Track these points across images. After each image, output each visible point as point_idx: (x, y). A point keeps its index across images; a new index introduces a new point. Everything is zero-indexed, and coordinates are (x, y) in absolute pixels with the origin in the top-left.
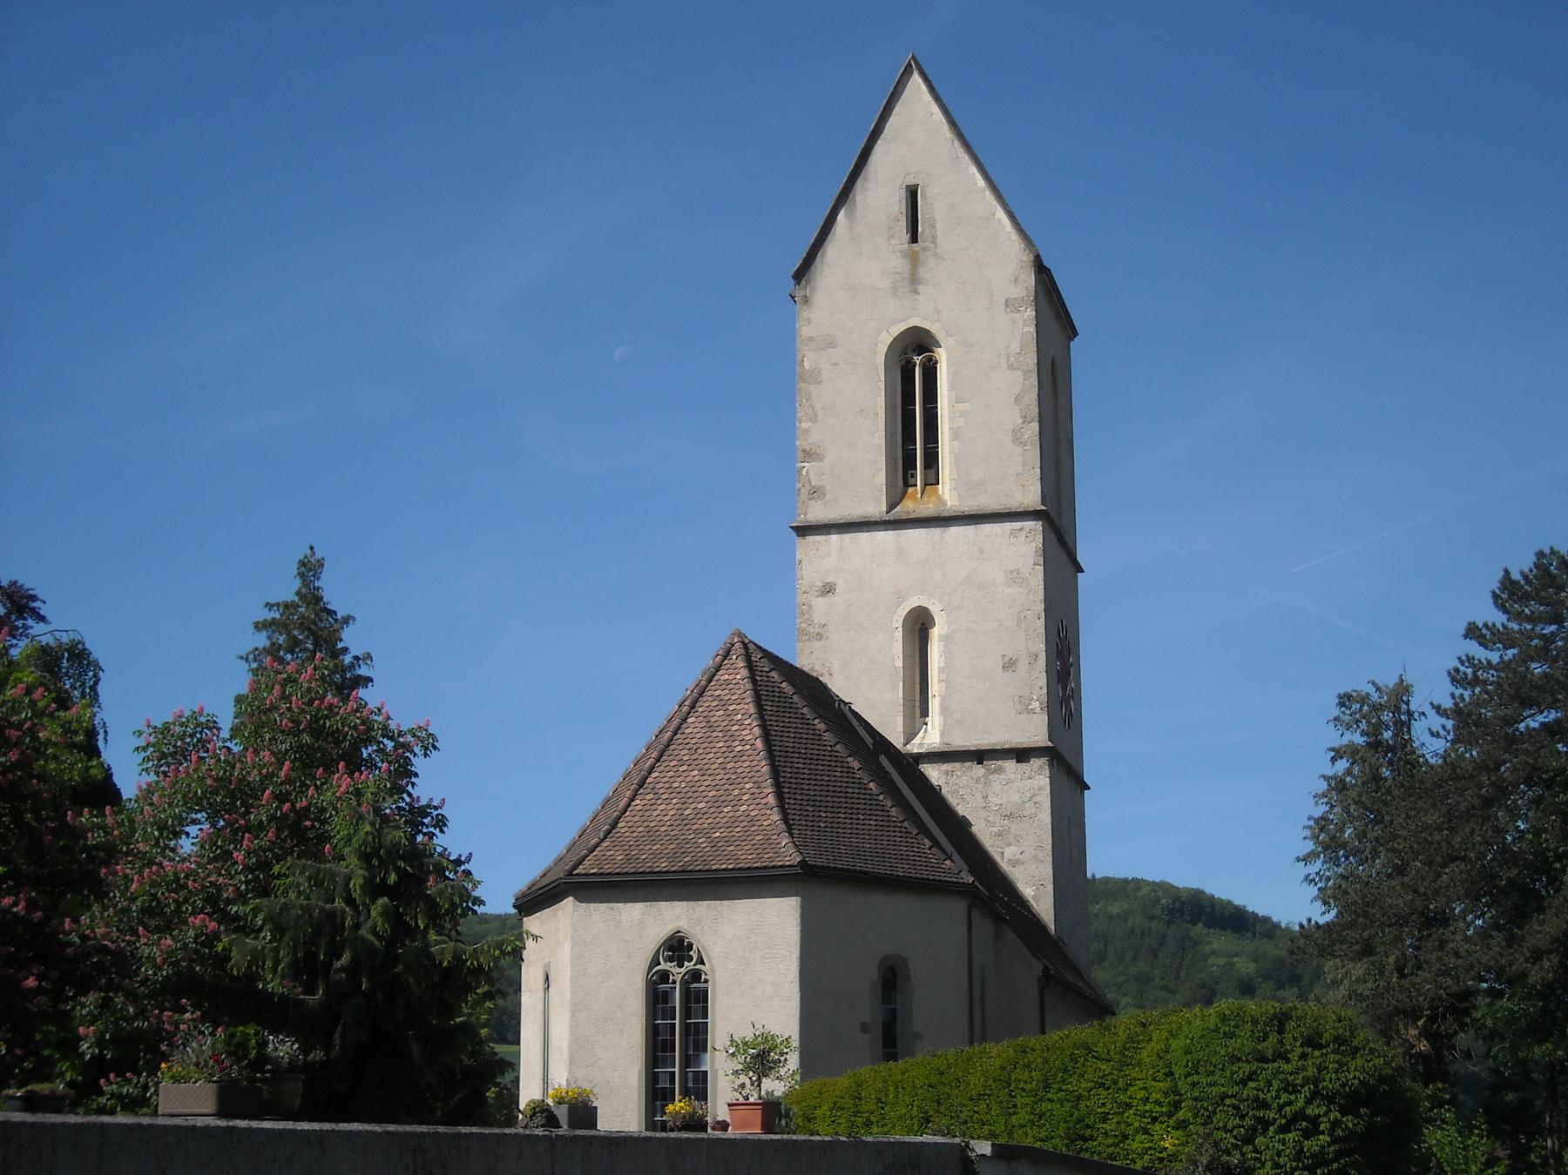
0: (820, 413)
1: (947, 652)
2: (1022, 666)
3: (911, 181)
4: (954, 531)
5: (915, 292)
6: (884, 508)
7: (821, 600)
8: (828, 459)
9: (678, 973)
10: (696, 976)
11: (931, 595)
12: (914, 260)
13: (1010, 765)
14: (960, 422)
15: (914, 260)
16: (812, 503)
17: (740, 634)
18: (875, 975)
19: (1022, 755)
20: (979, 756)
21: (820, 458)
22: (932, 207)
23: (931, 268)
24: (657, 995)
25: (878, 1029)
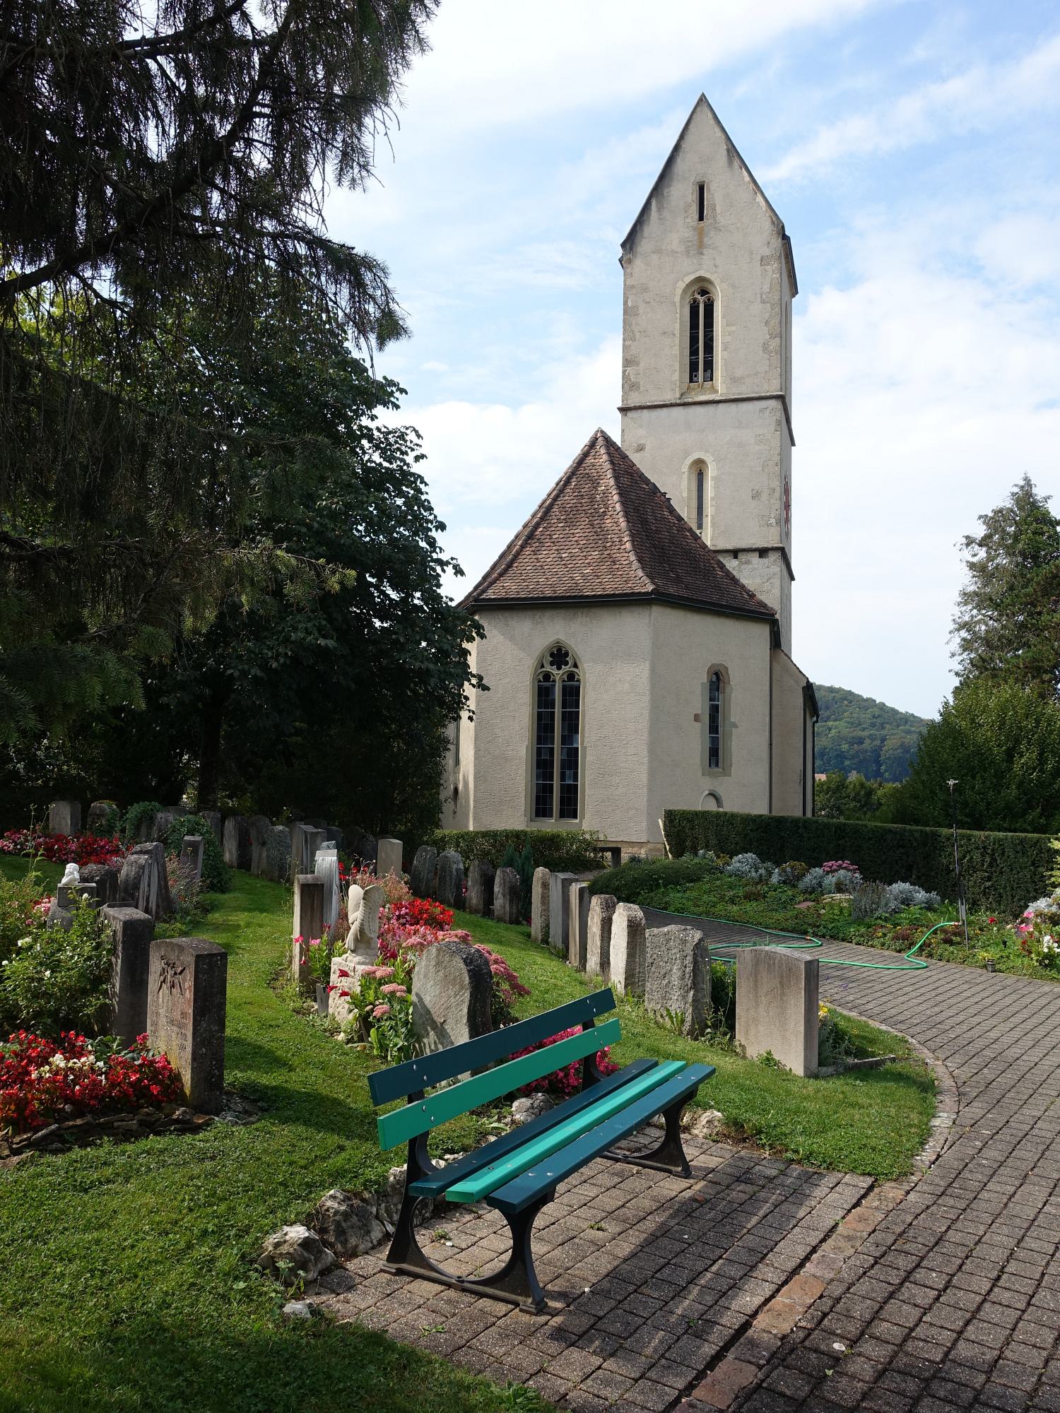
0: (638, 335)
1: (716, 487)
2: (764, 496)
3: (699, 179)
4: (721, 405)
6: (678, 395)
7: (638, 455)
8: (642, 365)
9: (558, 674)
10: (571, 676)
11: (707, 451)
12: (701, 234)
13: (754, 558)
14: (729, 339)
15: (701, 234)
17: (602, 432)
18: (704, 678)
19: (763, 552)
21: (638, 364)
22: (715, 196)
23: (713, 238)
24: (543, 693)
25: (706, 719)
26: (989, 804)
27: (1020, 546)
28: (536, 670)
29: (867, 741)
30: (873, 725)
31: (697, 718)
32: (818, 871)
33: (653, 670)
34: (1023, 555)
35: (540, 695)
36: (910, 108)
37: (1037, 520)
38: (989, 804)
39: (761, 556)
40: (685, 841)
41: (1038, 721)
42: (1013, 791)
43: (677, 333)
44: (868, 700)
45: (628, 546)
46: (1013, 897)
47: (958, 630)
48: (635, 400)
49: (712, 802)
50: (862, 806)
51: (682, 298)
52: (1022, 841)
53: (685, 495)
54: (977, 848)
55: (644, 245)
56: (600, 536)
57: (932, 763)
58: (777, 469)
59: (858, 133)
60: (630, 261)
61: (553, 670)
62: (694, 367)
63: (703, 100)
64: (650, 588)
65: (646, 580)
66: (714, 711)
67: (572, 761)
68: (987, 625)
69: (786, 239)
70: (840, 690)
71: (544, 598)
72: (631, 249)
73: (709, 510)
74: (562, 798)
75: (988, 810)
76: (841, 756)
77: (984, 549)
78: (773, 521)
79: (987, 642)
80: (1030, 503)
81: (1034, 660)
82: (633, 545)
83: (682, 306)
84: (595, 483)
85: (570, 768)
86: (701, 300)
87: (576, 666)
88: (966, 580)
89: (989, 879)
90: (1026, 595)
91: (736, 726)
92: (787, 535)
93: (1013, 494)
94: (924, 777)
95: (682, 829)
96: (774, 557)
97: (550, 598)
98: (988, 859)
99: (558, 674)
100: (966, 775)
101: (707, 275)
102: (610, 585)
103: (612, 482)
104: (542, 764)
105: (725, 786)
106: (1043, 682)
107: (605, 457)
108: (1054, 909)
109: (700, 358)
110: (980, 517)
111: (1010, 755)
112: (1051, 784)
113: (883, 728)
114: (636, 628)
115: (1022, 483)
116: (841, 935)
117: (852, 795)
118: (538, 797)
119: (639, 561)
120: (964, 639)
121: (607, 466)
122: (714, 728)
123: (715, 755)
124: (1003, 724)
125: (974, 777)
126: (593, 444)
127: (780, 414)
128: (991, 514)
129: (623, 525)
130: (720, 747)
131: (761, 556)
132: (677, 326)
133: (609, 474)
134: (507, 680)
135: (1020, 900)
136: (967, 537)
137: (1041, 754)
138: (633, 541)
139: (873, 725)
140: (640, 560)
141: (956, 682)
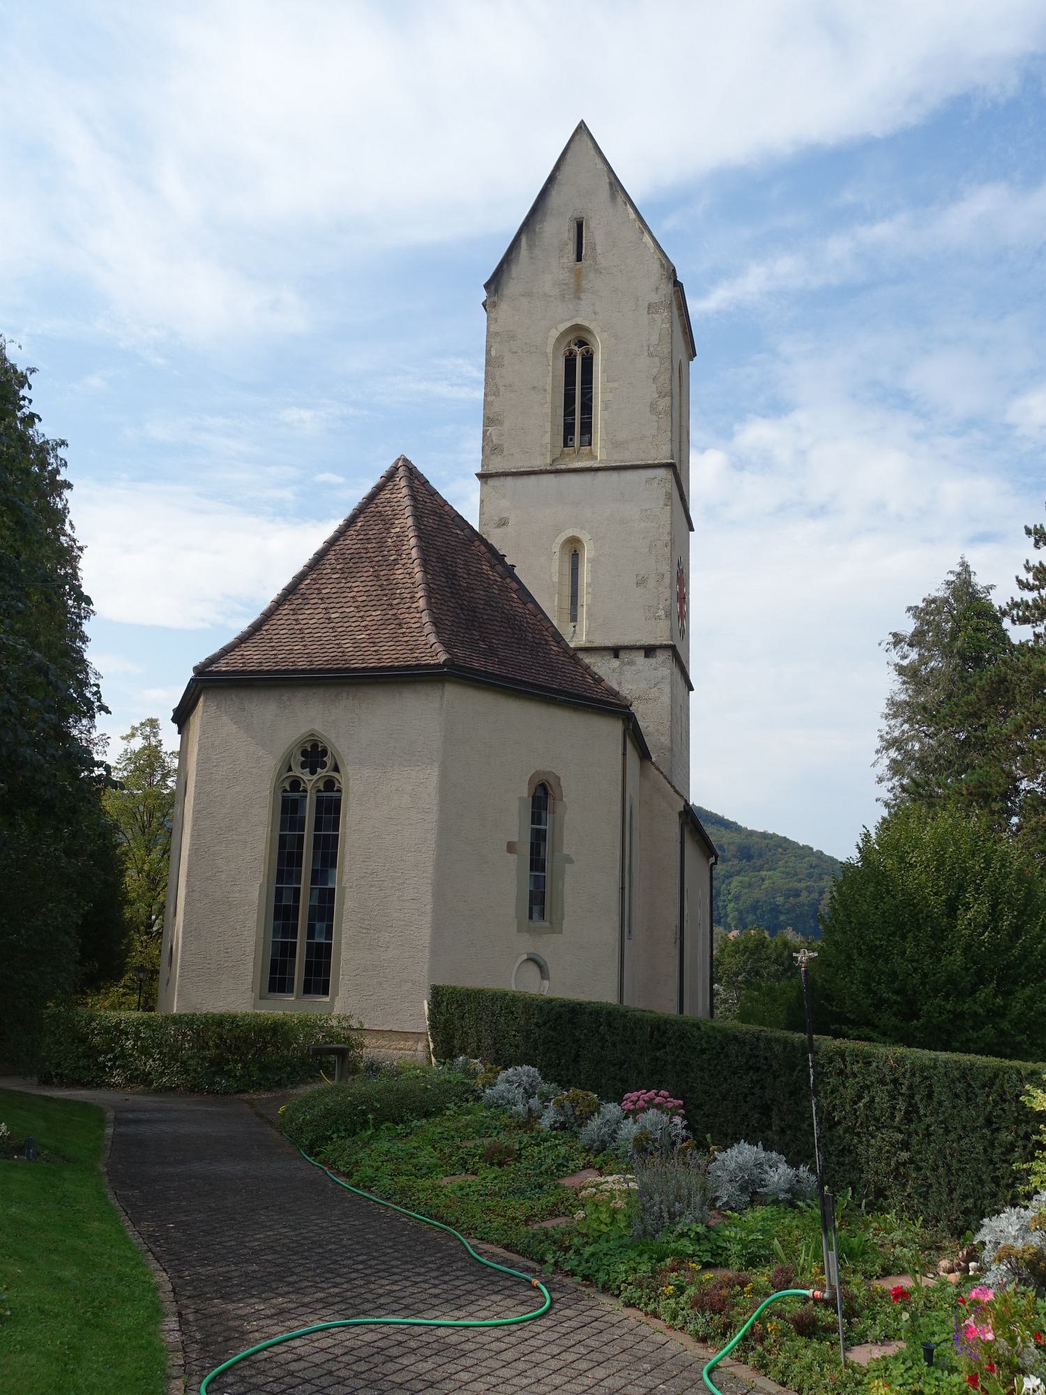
0: (502, 389)
1: (593, 571)
2: (652, 583)
4: (600, 474)
5: (579, 298)
6: (549, 461)
7: (500, 530)
9: (310, 781)
10: (330, 784)
11: (582, 528)
12: (578, 276)
13: (639, 658)
15: (578, 276)
16: (493, 457)
17: (405, 460)
18: (525, 791)
19: (649, 651)
20: (616, 651)
21: (501, 423)
22: (595, 234)
24: (289, 809)
25: (526, 850)
26: (925, 975)
27: (959, 643)
28: (279, 775)
29: (804, 894)
30: (810, 876)
31: (511, 848)
32: (612, 1110)
33: (444, 776)
34: (964, 658)
35: (284, 811)
36: (838, 248)
37: (979, 615)
38: (925, 975)
39: (647, 656)
40: (453, 1037)
41: (988, 861)
42: (956, 960)
43: (549, 388)
44: (805, 847)
45: (422, 603)
46: (951, 1191)
47: (887, 749)
48: (498, 465)
49: (533, 970)
50: (786, 970)
51: (556, 348)
52: (965, 1073)
53: (556, 579)
54: (882, 1082)
55: (512, 287)
56: (386, 591)
57: (848, 916)
58: (667, 550)
59: (786, 268)
60: (494, 305)
61: (305, 775)
62: (569, 429)
63: (582, 128)
64: (442, 657)
65: (438, 647)
66: (538, 839)
67: (325, 908)
68: (920, 741)
69: (678, 285)
70: (774, 836)
71: (294, 671)
72: (496, 291)
73: (585, 598)
74: (308, 964)
75: (923, 984)
76: (775, 910)
77: (916, 650)
78: (661, 613)
79: (922, 764)
80: (968, 593)
81: (981, 784)
82: (429, 603)
83: (555, 357)
84: (388, 523)
85: (322, 920)
86: (579, 351)
87: (336, 769)
88: (890, 685)
89: (906, 1146)
90: (968, 704)
91: (572, 862)
92: (684, 633)
93: (948, 583)
94: (838, 937)
95: (459, 1017)
96: (662, 656)
97: (303, 671)
98: (902, 1105)
99: (310, 781)
100: (893, 934)
101: (586, 324)
102: (390, 654)
103: (410, 522)
104: (282, 913)
105: (548, 947)
106: (992, 813)
107: (405, 491)
108: (1035, 1239)
109: (576, 416)
110: (909, 609)
111: (952, 908)
112: (1009, 949)
113: (821, 879)
114: (422, 715)
115: (958, 569)
116: (602, 1277)
117: (773, 957)
118: (274, 963)
119: (434, 624)
120: (894, 761)
121: (407, 502)
122: (537, 863)
123: (538, 902)
124: (941, 863)
125: (904, 938)
126: (390, 476)
127: (670, 485)
128: (922, 605)
129: (419, 576)
130: (547, 890)
131: (647, 656)
132: (549, 380)
133: (408, 512)
134: (238, 788)
135: (965, 1197)
136: (895, 635)
137: (994, 906)
138: (429, 598)
139: (810, 876)
140: (436, 623)
141: (885, 813)
